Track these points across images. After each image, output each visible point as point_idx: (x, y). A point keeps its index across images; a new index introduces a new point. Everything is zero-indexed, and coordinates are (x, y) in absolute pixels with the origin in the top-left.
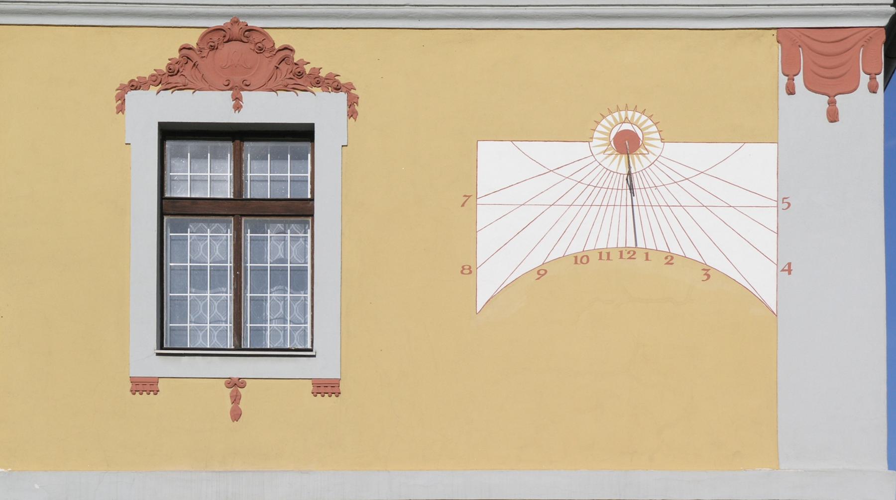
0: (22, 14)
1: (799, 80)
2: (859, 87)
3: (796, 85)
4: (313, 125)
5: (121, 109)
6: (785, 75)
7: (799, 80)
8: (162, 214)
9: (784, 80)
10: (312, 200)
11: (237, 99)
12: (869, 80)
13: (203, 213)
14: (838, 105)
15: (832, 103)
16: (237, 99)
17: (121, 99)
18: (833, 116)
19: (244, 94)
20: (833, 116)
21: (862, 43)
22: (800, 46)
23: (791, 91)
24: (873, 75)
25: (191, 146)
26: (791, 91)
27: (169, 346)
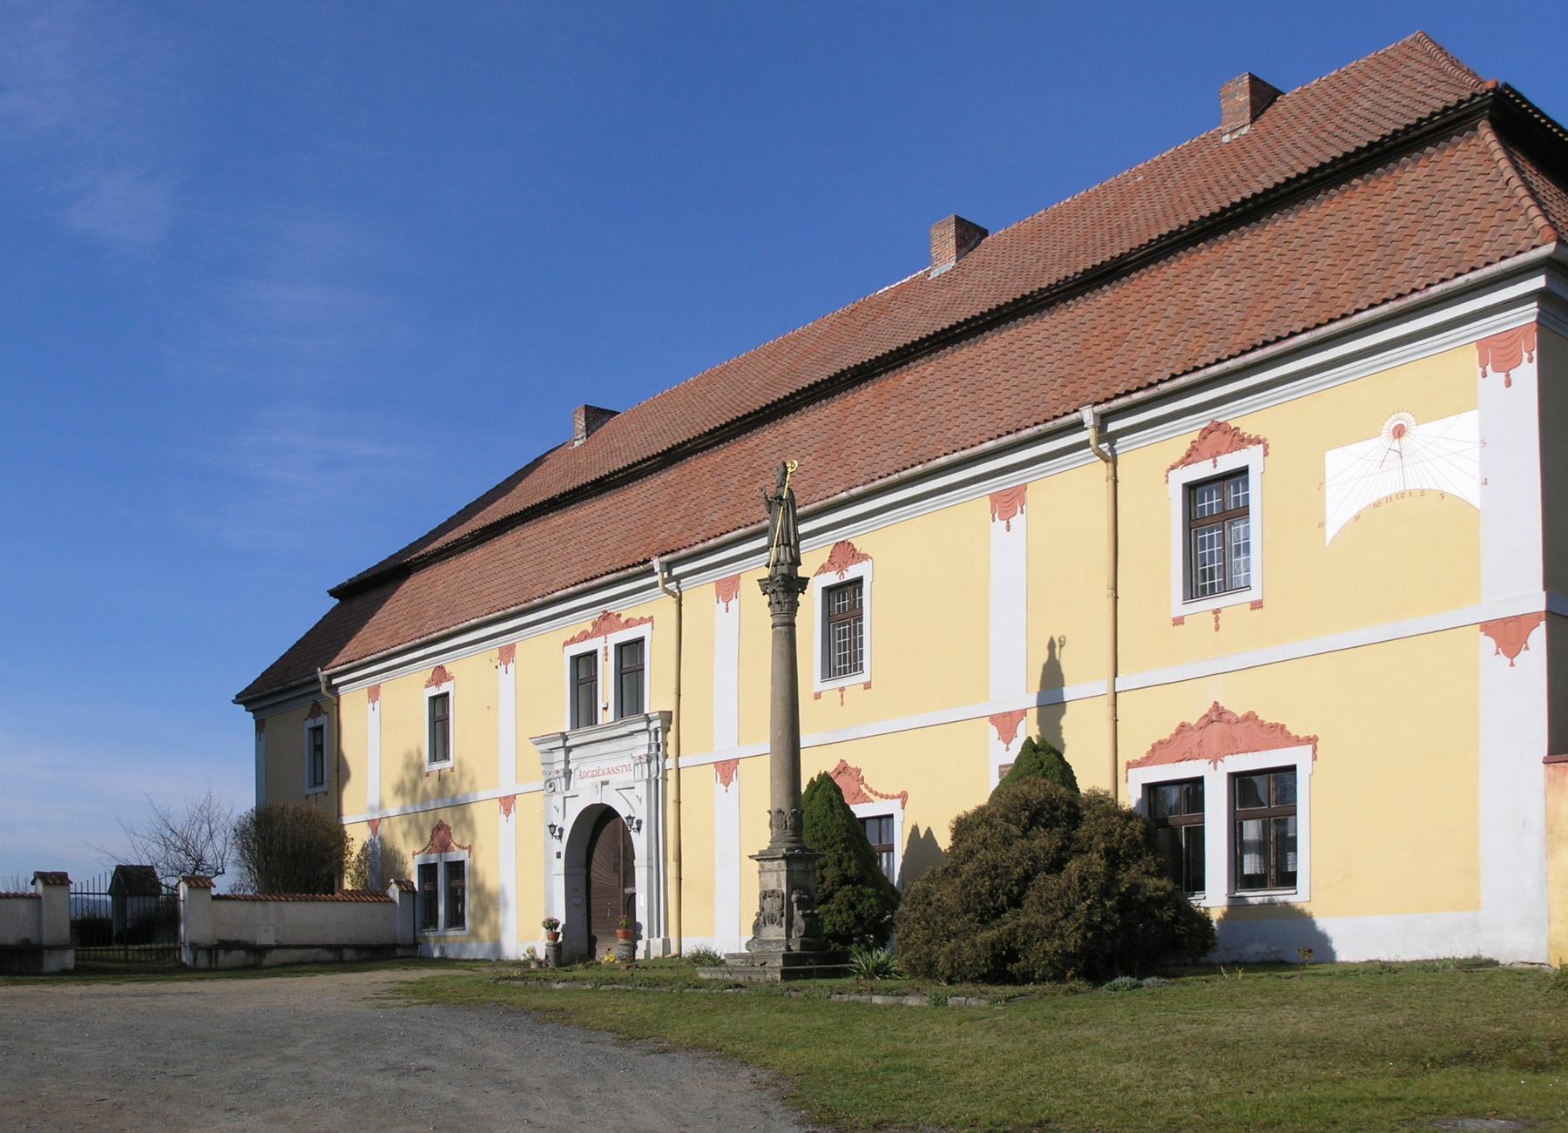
1: (1489, 368)
7: (1489, 368)
20: (1508, 383)
23: (718, 602)
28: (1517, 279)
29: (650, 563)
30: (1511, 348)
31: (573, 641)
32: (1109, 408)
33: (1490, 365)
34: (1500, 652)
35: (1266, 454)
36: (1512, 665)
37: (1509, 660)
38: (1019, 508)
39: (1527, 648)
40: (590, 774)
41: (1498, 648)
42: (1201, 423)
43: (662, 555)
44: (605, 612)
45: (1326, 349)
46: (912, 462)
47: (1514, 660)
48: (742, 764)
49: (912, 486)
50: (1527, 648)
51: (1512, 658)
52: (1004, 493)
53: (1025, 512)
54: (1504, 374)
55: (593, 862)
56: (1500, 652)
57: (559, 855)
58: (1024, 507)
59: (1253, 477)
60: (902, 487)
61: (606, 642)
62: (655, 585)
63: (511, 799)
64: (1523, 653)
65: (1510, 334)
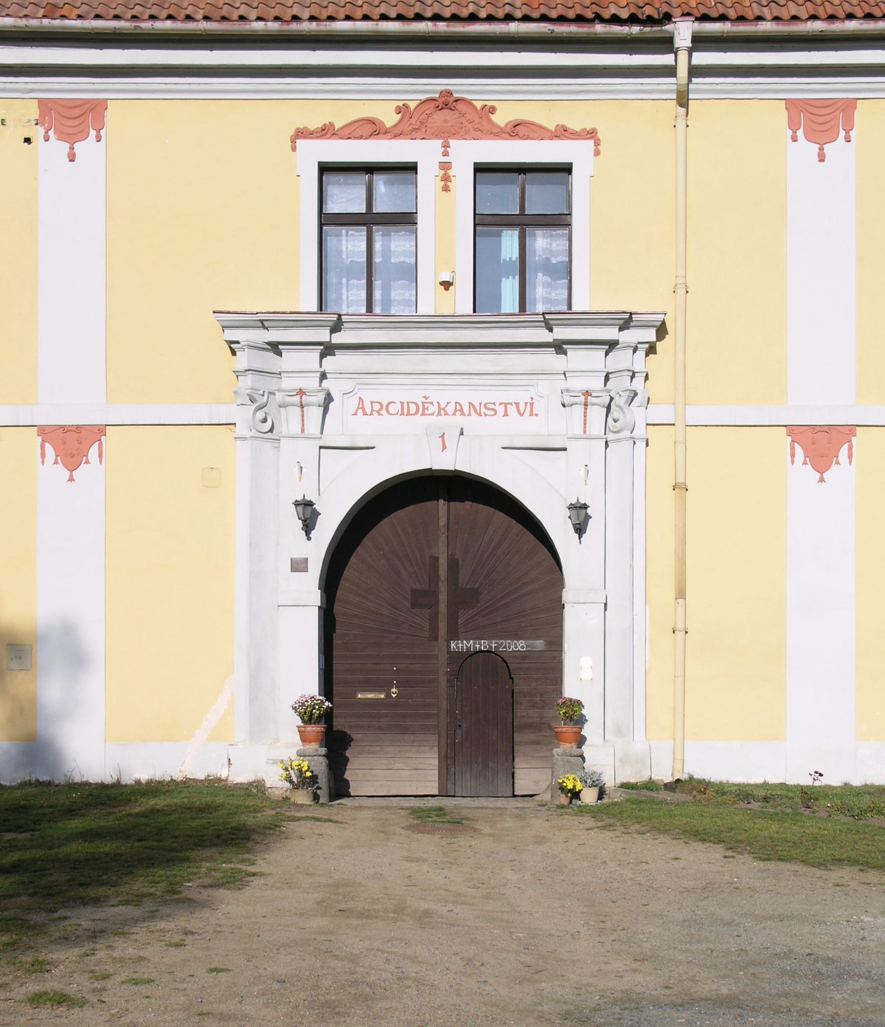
0: (648, 93)
1: (800, 133)
2: (37, 107)
3: (798, 136)
4: (417, 163)
5: (294, 149)
6: (844, 130)
7: (800, 133)
8: (321, 226)
9: (790, 132)
10: (416, 213)
11: (446, 146)
12: (845, 134)
13: (349, 222)
14: (825, 151)
15: (821, 149)
16: (446, 146)
17: (293, 141)
18: (822, 159)
19: (452, 142)
20: (822, 159)
21: (842, 108)
22: (802, 111)
23: (794, 139)
24: (848, 131)
25: (341, 178)
26: (794, 139)
27: (508, 312)
28: (435, 46)
29: (669, 27)
30: (830, 117)
31: (326, 132)
32: (552, 32)
33: (53, 129)
34: (59, 461)
35: (597, 153)
36: (822, 480)
37: (69, 473)
38: (842, 133)
39: (87, 462)
40: (393, 409)
41: (57, 456)
42: (426, 92)
43: (705, 18)
44: (450, 93)
45: (726, 50)
46: (331, 10)
47: (824, 475)
48: (111, 437)
49: (123, 48)
50: (87, 462)
51: (821, 473)
52: (817, 104)
53: (103, 139)
54: (818, 146)
55: (343, 583)
56: (59, 461)
57: (299, 566)
58: (103, 132)
59: (579, 179)
60: (91, 44)
61: (445, 154)
62: (670, 71)
63: (846, 430)
64: (834, 467)
65: (831, 102)
